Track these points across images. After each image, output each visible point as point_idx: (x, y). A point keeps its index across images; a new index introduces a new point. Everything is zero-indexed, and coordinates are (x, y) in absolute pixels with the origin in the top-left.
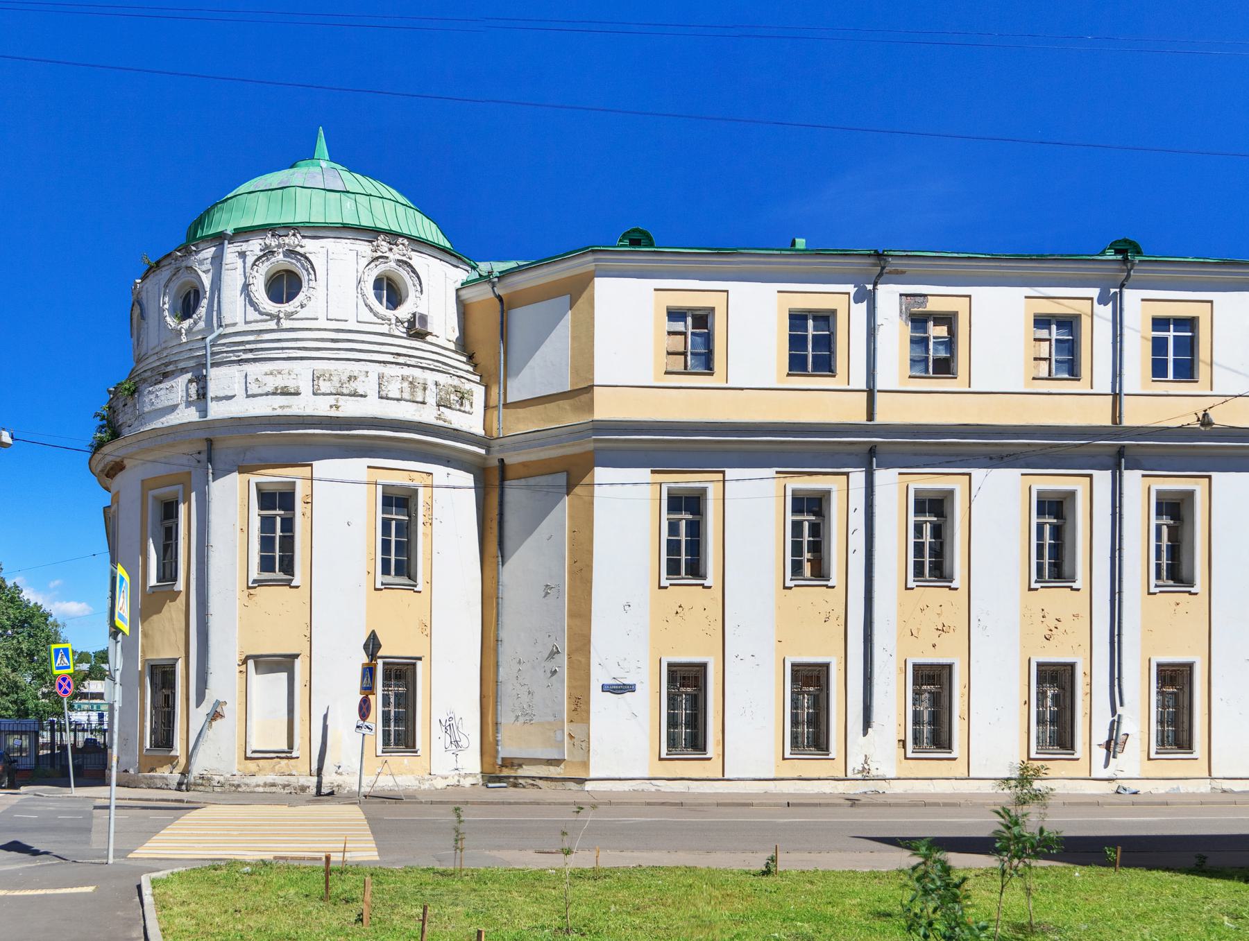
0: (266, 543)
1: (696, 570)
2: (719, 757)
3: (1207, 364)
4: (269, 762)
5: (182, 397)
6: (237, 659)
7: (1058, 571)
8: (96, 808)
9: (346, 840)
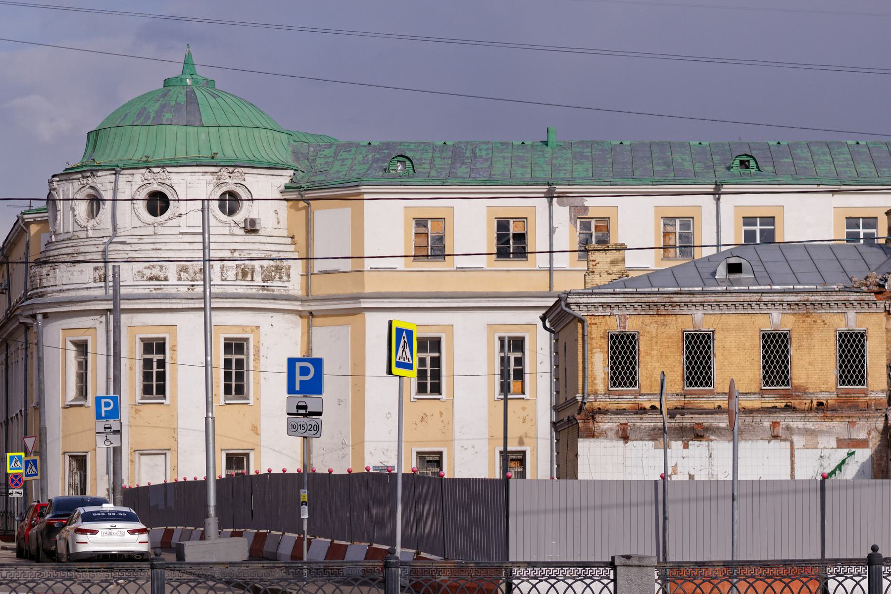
0: (147, 376)
1: (437, 389)
2: (685, 251)
6: (61, 452)
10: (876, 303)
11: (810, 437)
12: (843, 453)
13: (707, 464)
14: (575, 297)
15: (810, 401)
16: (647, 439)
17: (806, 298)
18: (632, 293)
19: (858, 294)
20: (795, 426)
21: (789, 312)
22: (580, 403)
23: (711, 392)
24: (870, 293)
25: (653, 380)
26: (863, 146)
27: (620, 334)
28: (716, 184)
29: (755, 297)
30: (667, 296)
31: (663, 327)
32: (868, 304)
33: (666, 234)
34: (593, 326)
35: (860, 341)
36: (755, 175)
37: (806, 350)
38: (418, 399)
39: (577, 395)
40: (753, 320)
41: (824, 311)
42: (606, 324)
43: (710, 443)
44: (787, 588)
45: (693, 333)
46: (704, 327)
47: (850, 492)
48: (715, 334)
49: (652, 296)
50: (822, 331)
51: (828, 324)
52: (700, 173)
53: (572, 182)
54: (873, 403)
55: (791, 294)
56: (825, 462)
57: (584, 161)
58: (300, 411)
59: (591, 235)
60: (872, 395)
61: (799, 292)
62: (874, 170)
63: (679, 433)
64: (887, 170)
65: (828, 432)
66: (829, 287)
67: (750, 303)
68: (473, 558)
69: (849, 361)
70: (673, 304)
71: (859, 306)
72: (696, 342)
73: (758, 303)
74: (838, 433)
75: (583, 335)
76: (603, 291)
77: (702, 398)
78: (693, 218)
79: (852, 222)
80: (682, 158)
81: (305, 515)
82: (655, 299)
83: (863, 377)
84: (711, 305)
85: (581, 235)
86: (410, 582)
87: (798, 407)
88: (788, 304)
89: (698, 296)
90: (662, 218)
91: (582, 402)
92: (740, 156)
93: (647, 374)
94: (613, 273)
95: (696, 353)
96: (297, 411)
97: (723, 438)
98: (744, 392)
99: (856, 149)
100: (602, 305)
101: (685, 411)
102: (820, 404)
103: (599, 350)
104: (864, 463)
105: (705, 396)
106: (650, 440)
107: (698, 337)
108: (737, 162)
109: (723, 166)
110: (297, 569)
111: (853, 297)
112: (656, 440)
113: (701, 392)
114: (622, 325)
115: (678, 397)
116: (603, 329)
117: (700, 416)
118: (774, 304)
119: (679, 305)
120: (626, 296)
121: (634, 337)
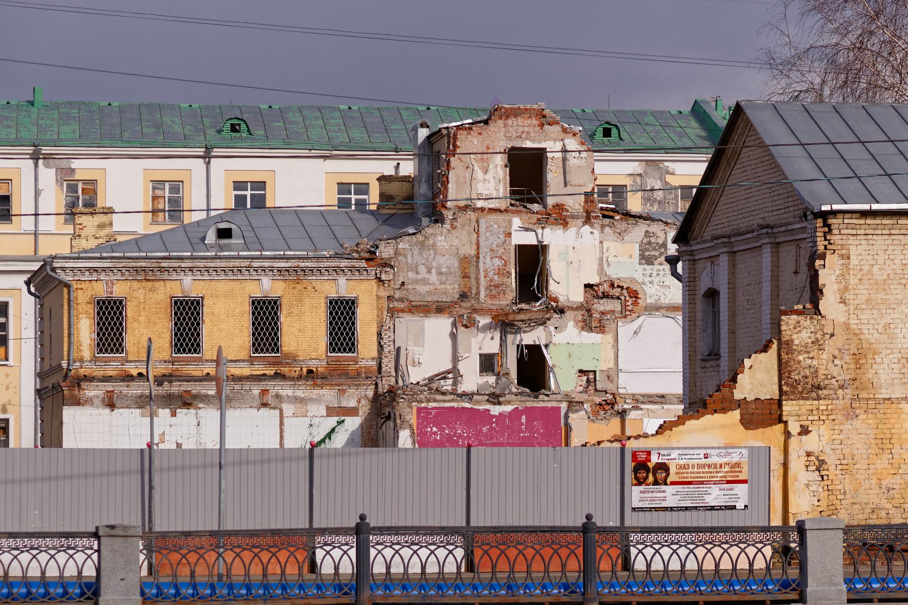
3: (834, 178)
7: (572, 309)
8: (596, 160)
11: (299, 405)
12: (333, 421)
15: (299, 369)
17: (296, 264)
18: (119, 258)
20: (284, 394)
21: (279, 278)
23: (200, 360)
25: (140, 346)
33: (155, 198)
36: (246, 138)
41: (314, 278)
42: (93, 289)
43: (199, 411)
52: (190, 136)
56: (315, 430)
59: (78, 198)
61: (289, 258)
62: (365, 135)
65: (318, 400)
66: (319, 253)
70: (162, 270)
71: (349, 273)
72: (184, 309)
75: (69, 301)
76: (90, 255)
78: (182, 182)
79: (343, 188)
82: (144, 264)
83: (353, 344)
87: (287, 374)
91: (67, 369)
98: (234, 359)
99: (348, 114)
100: (89, 269)
101: (173, 378)
102: (310, 372)
106: (137, 408)
107: (187, 303)
108: (228, 125)
113: (189, 359)
114: (109, 290)
121: (121, 302)
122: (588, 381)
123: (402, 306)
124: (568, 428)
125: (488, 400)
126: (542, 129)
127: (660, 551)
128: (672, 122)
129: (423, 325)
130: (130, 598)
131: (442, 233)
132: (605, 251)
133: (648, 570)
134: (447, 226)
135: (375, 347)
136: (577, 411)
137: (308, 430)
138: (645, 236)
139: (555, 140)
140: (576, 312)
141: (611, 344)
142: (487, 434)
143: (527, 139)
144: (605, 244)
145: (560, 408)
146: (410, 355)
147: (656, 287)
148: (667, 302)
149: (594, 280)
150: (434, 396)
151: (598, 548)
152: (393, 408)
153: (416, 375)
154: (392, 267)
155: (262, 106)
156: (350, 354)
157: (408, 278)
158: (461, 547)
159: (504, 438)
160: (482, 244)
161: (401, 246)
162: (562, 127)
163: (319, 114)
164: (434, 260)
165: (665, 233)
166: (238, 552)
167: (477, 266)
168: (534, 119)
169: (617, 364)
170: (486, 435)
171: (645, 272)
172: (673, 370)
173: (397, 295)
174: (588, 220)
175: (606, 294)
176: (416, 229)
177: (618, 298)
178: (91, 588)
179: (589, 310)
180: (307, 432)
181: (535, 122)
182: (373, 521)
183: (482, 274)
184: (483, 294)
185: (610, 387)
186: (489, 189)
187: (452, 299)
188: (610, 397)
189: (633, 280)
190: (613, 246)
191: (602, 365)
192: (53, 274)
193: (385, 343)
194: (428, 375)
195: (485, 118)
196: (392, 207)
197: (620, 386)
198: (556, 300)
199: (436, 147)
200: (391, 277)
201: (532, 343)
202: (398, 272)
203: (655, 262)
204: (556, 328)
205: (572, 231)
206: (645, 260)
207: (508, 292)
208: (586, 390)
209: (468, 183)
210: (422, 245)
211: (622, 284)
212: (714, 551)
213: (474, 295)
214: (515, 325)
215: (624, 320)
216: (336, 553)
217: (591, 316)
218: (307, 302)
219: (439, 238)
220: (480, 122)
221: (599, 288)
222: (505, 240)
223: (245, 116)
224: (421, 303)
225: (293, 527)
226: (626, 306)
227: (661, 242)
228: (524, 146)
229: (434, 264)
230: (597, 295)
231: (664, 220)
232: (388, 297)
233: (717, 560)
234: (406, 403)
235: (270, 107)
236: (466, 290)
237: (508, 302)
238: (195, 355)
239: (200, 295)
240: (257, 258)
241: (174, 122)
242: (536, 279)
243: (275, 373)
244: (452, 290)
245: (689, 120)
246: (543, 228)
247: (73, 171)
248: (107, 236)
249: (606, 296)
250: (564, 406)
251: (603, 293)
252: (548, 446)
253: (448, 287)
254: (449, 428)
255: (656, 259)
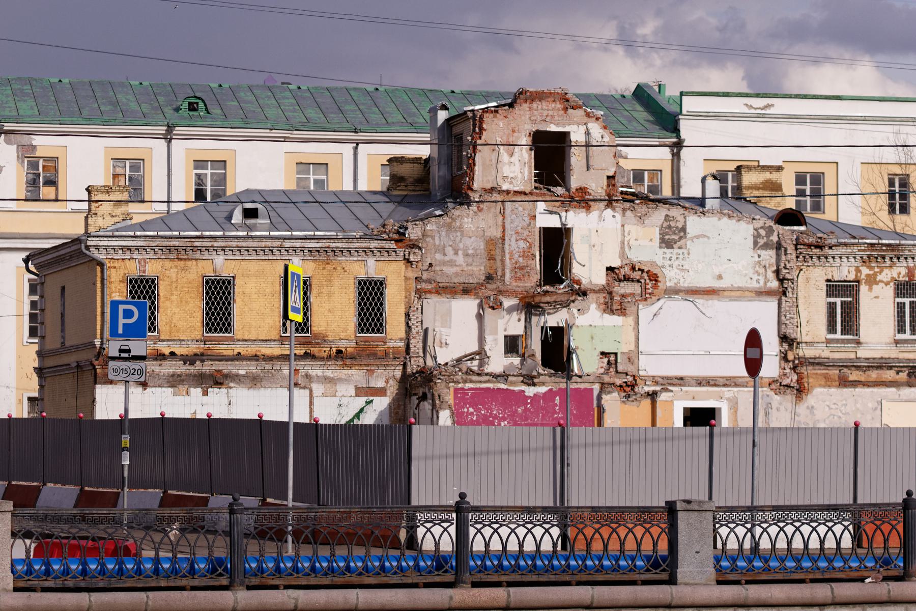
4: (779, 542)
5: (247, 351)
7: (594, 291)
9: (676, 200)
10: (396, 252)
11: (328, 385)
12: (361, 401)
13: (227, 411)
14: (95, 239)
15: (329, 349)
16: (165, 385)
17: (327, 245)
18: (153, 237)
19: (379, 242)
20: (314, 374)
21: (310, 258)
22: (98, 348)
23: (232, 339)
24: (391, 240)
25: (173, 325)
26: (305, 91)
27: (139, 279)
28: (168, 126)
29: (277, 243)
30: (189, 240)
31: (183, 272)
32: (388, 251)
33: (115, 176)
34: (112, 270)
35: (379, 289)
36: (206, 117)
37: (326, 297)
38: (30, 343)
39: (95, 340)
40: (274, 266)
41: (344, 259)
42: (126, 268)
43: (230, 390)
44: (765, 533)
45: (213, 278)
46: (224, 272)
47: (730, 439)
48: (236, 280)
49: (173, 240)
50: (342, 278)
51: (348, 271)
52: (148, 114)
53: (21, 120)
54: (391, 351)
55: (312, 241)
56: (343, 410)
57: (26, 98)
58: (123, 355)
59: (39, 175)
60: (390, 344)
61: (320, 239)
62: (322, 116)
63: (199, 380)
64: (335, 116)
65: (347, 380)
66: (349, 234)
67: (271, 249)
68: (348, 502)
69: (368, 309)
70: (194, 249)
71: (378, 254)
72: (216, 288)
73: (279, 249)
74: (356, 382)
75: (103, 279)
76: (124, 233)
77: (222, 344)
78: (143, 160)
79: (303, 166)
80: (126, 98)
81: (126, 462)
82: (177, 243)
83: (381, 325)
84: (232, 250)
85: (28, 175)
86: (255, 530)
87: (317, 355)
88: (309, 251)
89: (219, 241)
90: (112, 159)
91: (100, 347)
92: (189, 97)
93: (166, 319)
94: (116, 216)
95: (216, 299)
96: (120, 355)
97: (242, 385)
98: (264, 338)
99: (299, 94)
100: (123, 248)
101: (204, 358)
102: (339, 352)
103: (118, 294)
104: (381, 411)
105: (225, 343)
106: (169, 387)
107: (218, 283)
108: (186, 104)
109: (170, 108)
110: (77, 516)
111: (374, 244)
112: (175, 387)
113: (221, 338)
114: (142, 269)
115: (198, 343)
116: (122, 272)
117: (220, 363)
118: (295, 250)
119: (200, 250)
120: (147, 239)
121: (153, 281)
122: (609, 363)
123: (429, 287)
124: (601, 410)
125: (522, 382)
126: (566, 113)
127: (735, 530)
128: (617, 105)
129: (450, 307)
130: (705, 569)
131: (468, 214)
132: (626, 234)
133: (789, 549)
134: (474, 207)
135: (403, 327)
136: (609, 393)
137: (337, 410)
138: (665, 220)
139: (578, 124)
140: (598, 295)
141: (632, 327)
142: (522, 415)
143: (551, 123)
144: (627, 228)
145: (592, 389)
146: (437, 336)
147: (676, 270)
148: (686, 285)
149: (616, 263)
150: (470, 377)
151: (470, 527)
152: (430, 388)
153: (444, 356)
154: (420, 248)
155: (212, 85)
156: (378, 335)
157: (436, 259)
158: (556, 525)
159: (538, 419)
160: (507, 226)
161: (429, 227)
162: (585, 111)
163: (270, 94)
164: (461, 241)
165: (685, 218)
166: (614, 527)
167: (503, 248)
168: (558, 103)
169: (637, 346)
170: (520, 416)
171: (664, 256)
172: (692, 353)
173: (425, 276)
174: (610, 202)
175: (627, 277)
176: (443, 211)
177: (638, 281)
178: (666, 561)
179: (610, 293)
180: (336, 412)
181: (559, 106)
182: (473, 500)
183: (507, 256)
184: (508, 276)
185: (631, 369)
186: (514, 172)
187: (478, 281)
188: (630, 378)
189: (653, 263)
190: (634, 230)
191: (623, 347)
192: (87, 252)
193: (413, 324)
194: (457, 355)
195: (510, 101)
196: (404, 188)
197: (640, 368)
198: (578, 282)
199: (456, 130)
200: (419, 258)
201: (556, 325)
202: (425, 253)
203: (674, 246)
204: (579, 310)
205: (594, 214)
206: (665, 243)
207: (533, 275)
208: (607, 372)
209: (494, 166)
210: (449, 227)
211: (643, 267)
212: (602, 531)
213: (499, 277)
214: (540, 307)
215: (644, 302)
216: (437, 530)
217: (612, 299)
218: (337, 282)
219: (466, 220)
220: (504, 105)
221: (620, 270)
222: (530, 223)
223: (198, 95)
224: (448, 285)
225: (621, 505)
226: (646, 289)
227: (680, 226)
228: (548, 129)
229: (461, 246)
230: (618, 278)
231: (682, 204)
232: (416, 278)
233: (487, 540)
234: (444, 384)
235: (221, 86)
236: (491, 272)
237: (532, 284)
238: (227, 335)
239: (231, 275)
240: (289, 239)
241: (129, 100)
242: (560, 261)
243: (305, 353)
244: (478, 271)
245: (634, 104)
246: (566, 211)
247: (34, 148)
248: (123, 214)
249: (627, 279)
250: (596, 387)
251: (624, 276)
252: (582, 426)
253: (475, 269)
254: (485, 408)
255: (675, 243)
